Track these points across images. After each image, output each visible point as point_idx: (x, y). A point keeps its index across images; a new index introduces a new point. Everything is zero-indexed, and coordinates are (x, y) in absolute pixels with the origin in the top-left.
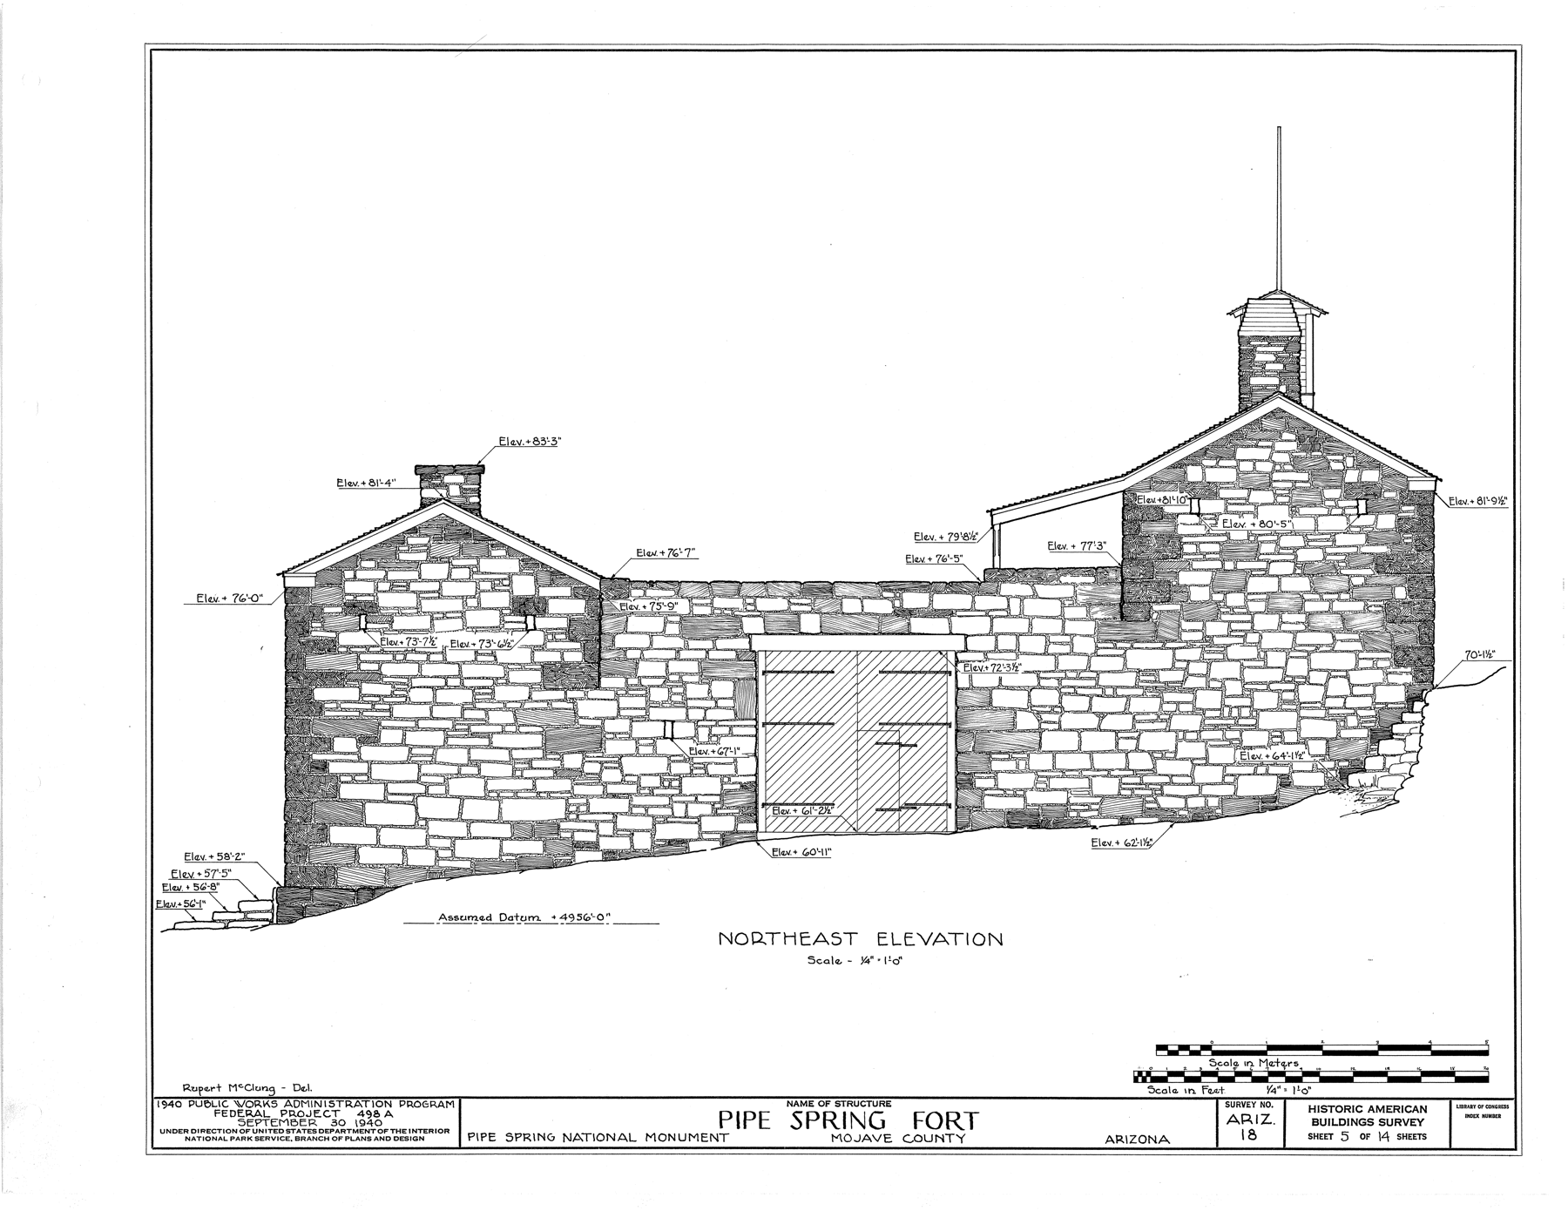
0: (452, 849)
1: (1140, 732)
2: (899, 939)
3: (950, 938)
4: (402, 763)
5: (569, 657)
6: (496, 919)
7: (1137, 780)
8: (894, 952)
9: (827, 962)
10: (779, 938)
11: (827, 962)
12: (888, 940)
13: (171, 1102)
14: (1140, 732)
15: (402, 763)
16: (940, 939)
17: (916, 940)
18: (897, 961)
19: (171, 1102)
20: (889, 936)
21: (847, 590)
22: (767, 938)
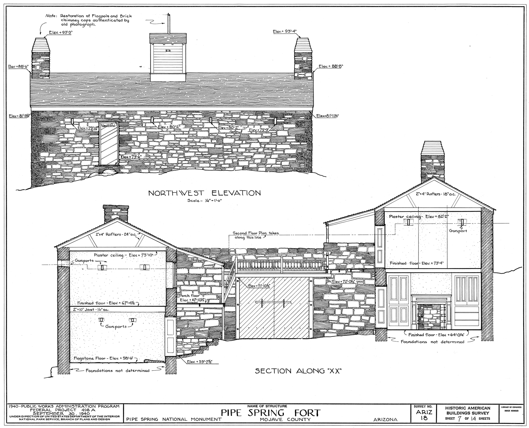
0: (360, 305)
1: (93, 157)
2: (222, 193)
3: (241, 193)
4: (216, 274)
5: (46, 154)
6: (294, 371)
7: (62, 167)
8: (218, 198)
9: (194, 201)
10: (171, 193)
11: (194, 201)
12: (217, 194)
13: (373, 298)
14: (93, 157)
15: (216, 274)
16: (237, 193)
17: (228, 193)
18: (219, 201)
19: (373, 298)
20: (217, 192)
21: (50, 182)
22: (167, 193)
